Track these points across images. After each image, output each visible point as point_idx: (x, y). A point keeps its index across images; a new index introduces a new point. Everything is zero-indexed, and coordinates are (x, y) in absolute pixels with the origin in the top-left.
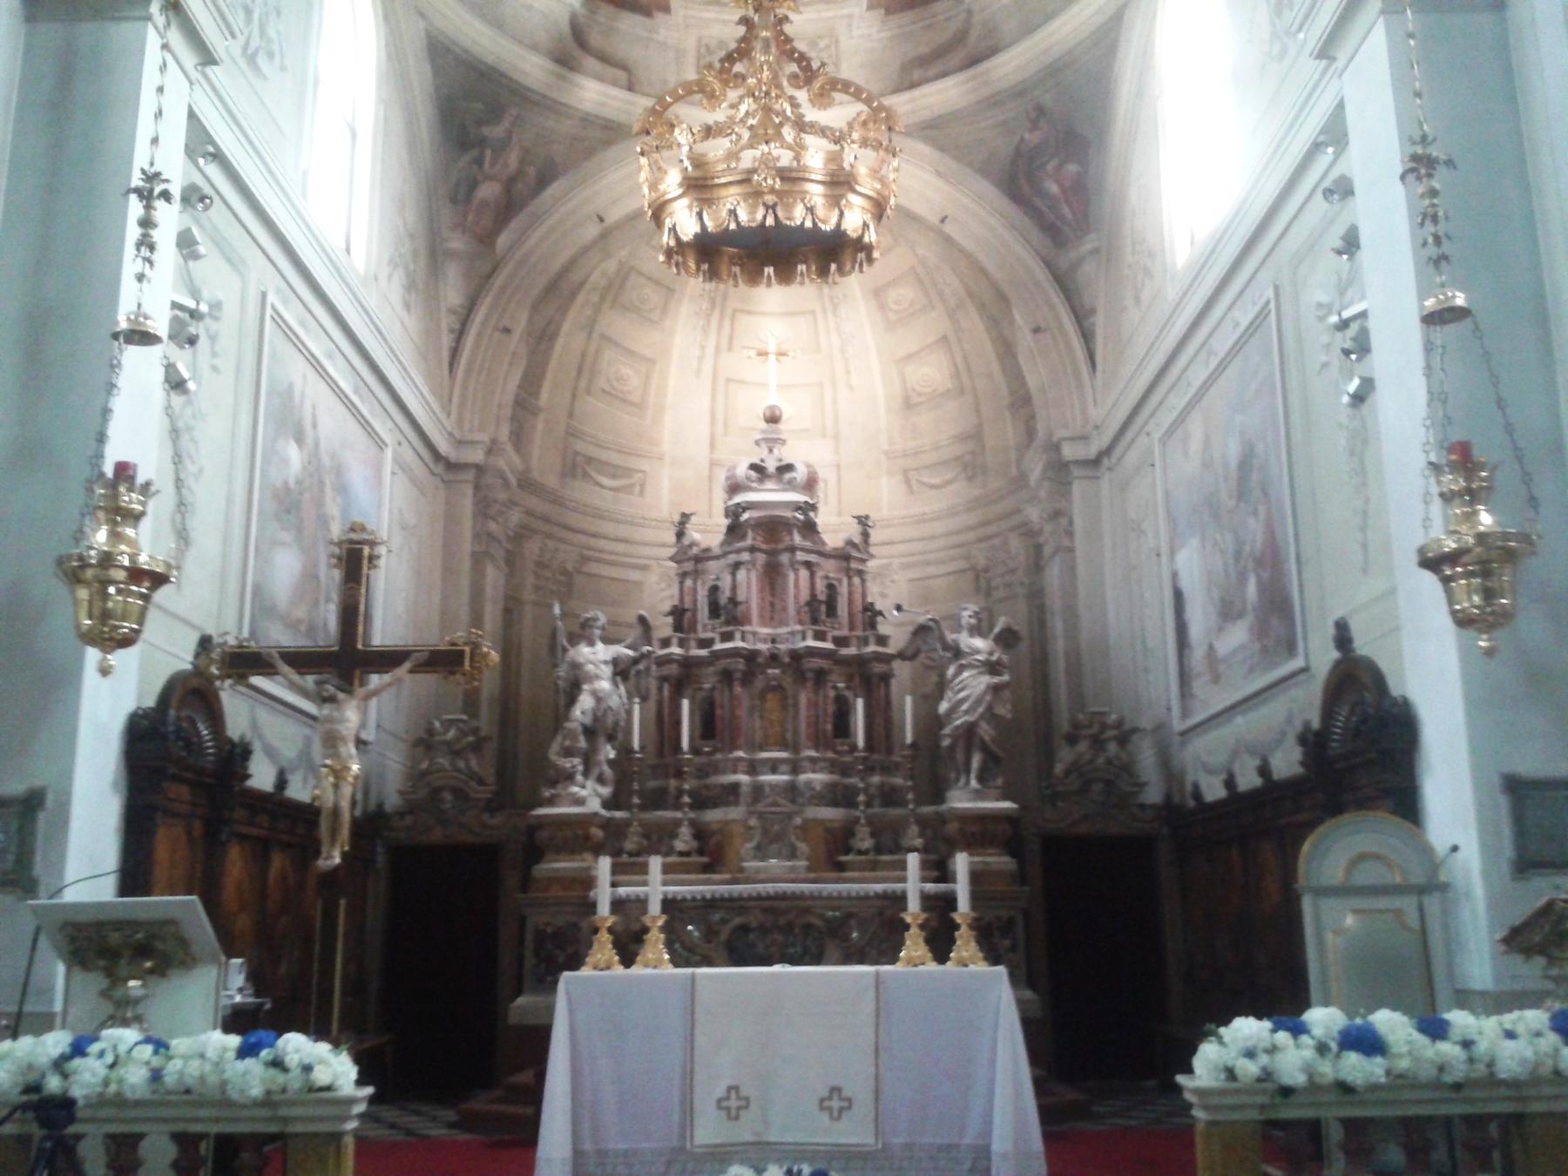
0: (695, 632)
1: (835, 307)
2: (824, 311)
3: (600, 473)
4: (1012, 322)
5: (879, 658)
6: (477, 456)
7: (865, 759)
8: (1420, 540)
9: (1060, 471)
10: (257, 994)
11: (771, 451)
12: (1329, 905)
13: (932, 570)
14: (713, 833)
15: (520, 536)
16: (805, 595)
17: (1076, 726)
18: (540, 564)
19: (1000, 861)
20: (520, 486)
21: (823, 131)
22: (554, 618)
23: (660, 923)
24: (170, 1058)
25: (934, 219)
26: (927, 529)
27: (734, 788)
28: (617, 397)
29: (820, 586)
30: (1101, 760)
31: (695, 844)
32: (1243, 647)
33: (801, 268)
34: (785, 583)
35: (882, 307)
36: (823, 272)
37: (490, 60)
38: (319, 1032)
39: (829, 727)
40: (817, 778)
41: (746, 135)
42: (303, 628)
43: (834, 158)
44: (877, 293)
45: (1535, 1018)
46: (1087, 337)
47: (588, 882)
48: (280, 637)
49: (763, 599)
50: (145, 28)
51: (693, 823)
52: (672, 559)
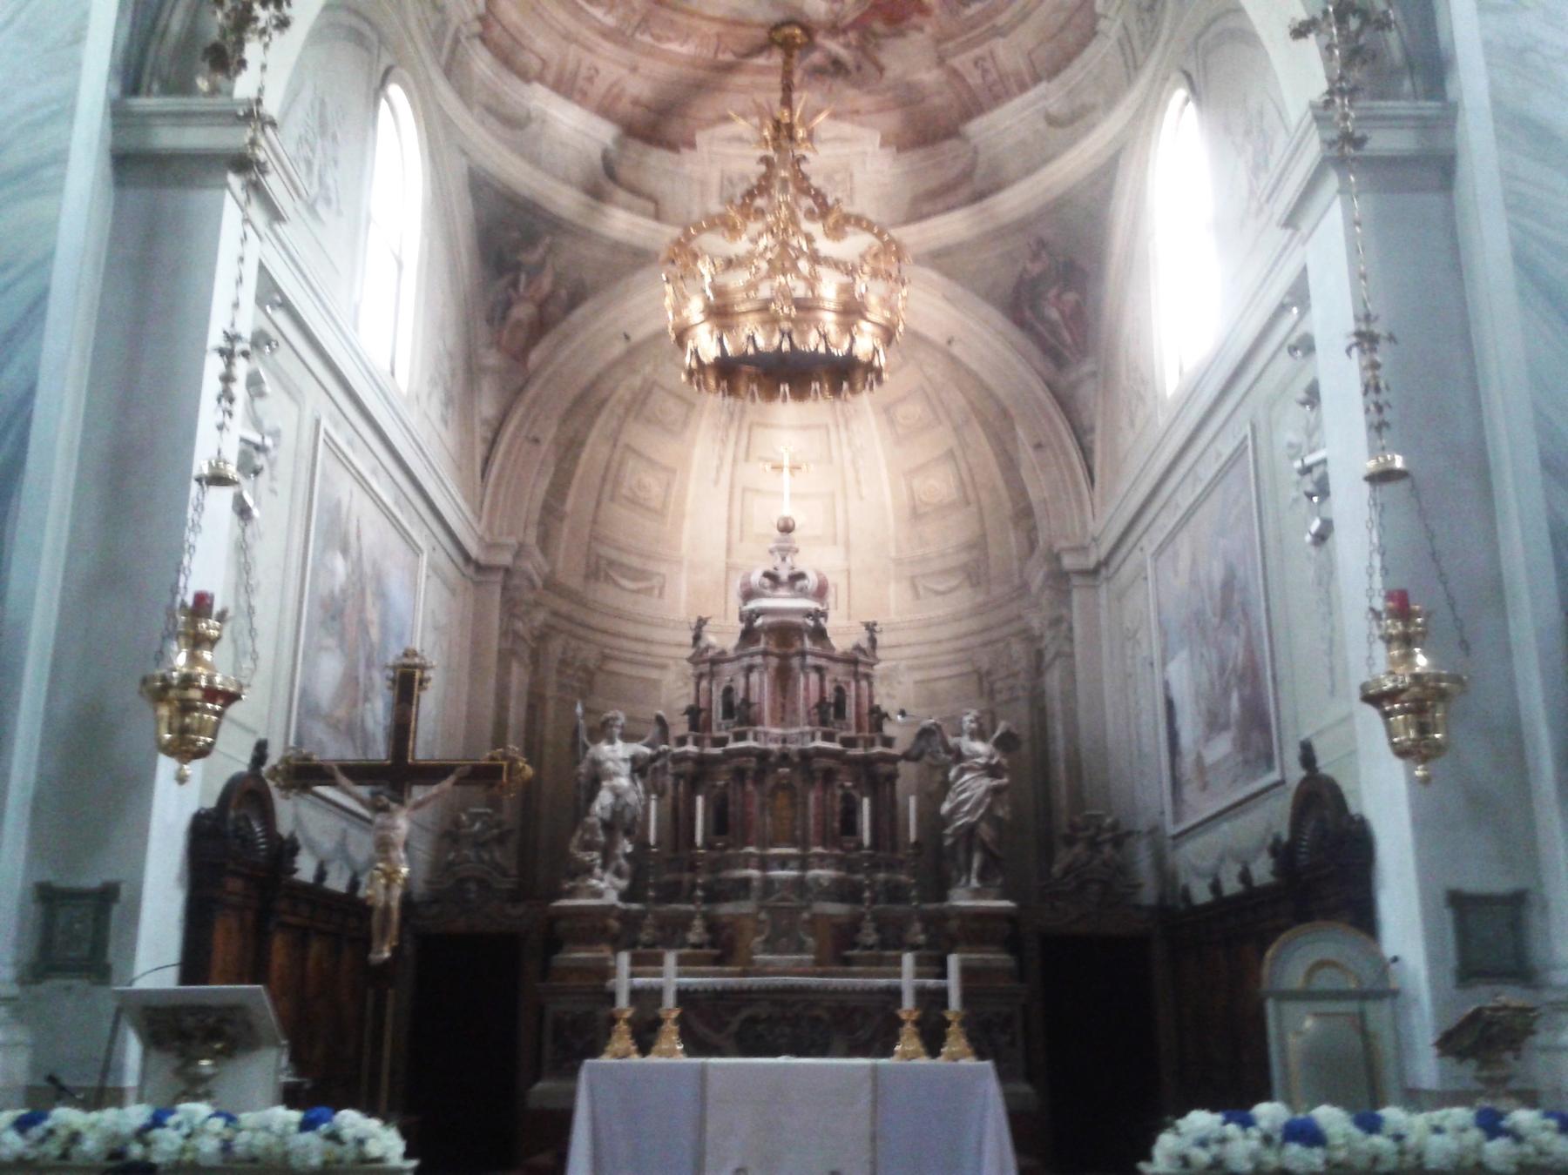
3: (623, 576)
4: (1014, 439)
5: (885, 758)
6: (505, 558)
7: (871, 856)
8: (1364, 677)
9: (1060, 580)
10: (297, 1074)
11: (784, 559)
12: (1290, 1008)
13: (935, 673)
15: (543, 637)
16: (814, 698)
17: (1073, 826)
18: (563, 662)
19: (998, 958)
21: (836, 264)
22: (576, 716)
23: (674, 1015)
24: (240, 1130)
25: (942, 341)
27: (746, 882)
29: (829, 688)
31: (707, 937)
32: (1226, 758)
33: (815, 386)
35: (891, 422)
36: (836, 390)
37: (525, 192)
38: (370, 1110)
39: (837, 825)
40: (823, 874)
41: (764, 266)
42: (342, 727)
43: (847, 289)
44: (887, 410)
45: (1460, 1115)
46: (1086, 453)
47: (606, 972)
48: (331, 749)
50: (223, 197)
51: (705, 916)
52: (690, 660)
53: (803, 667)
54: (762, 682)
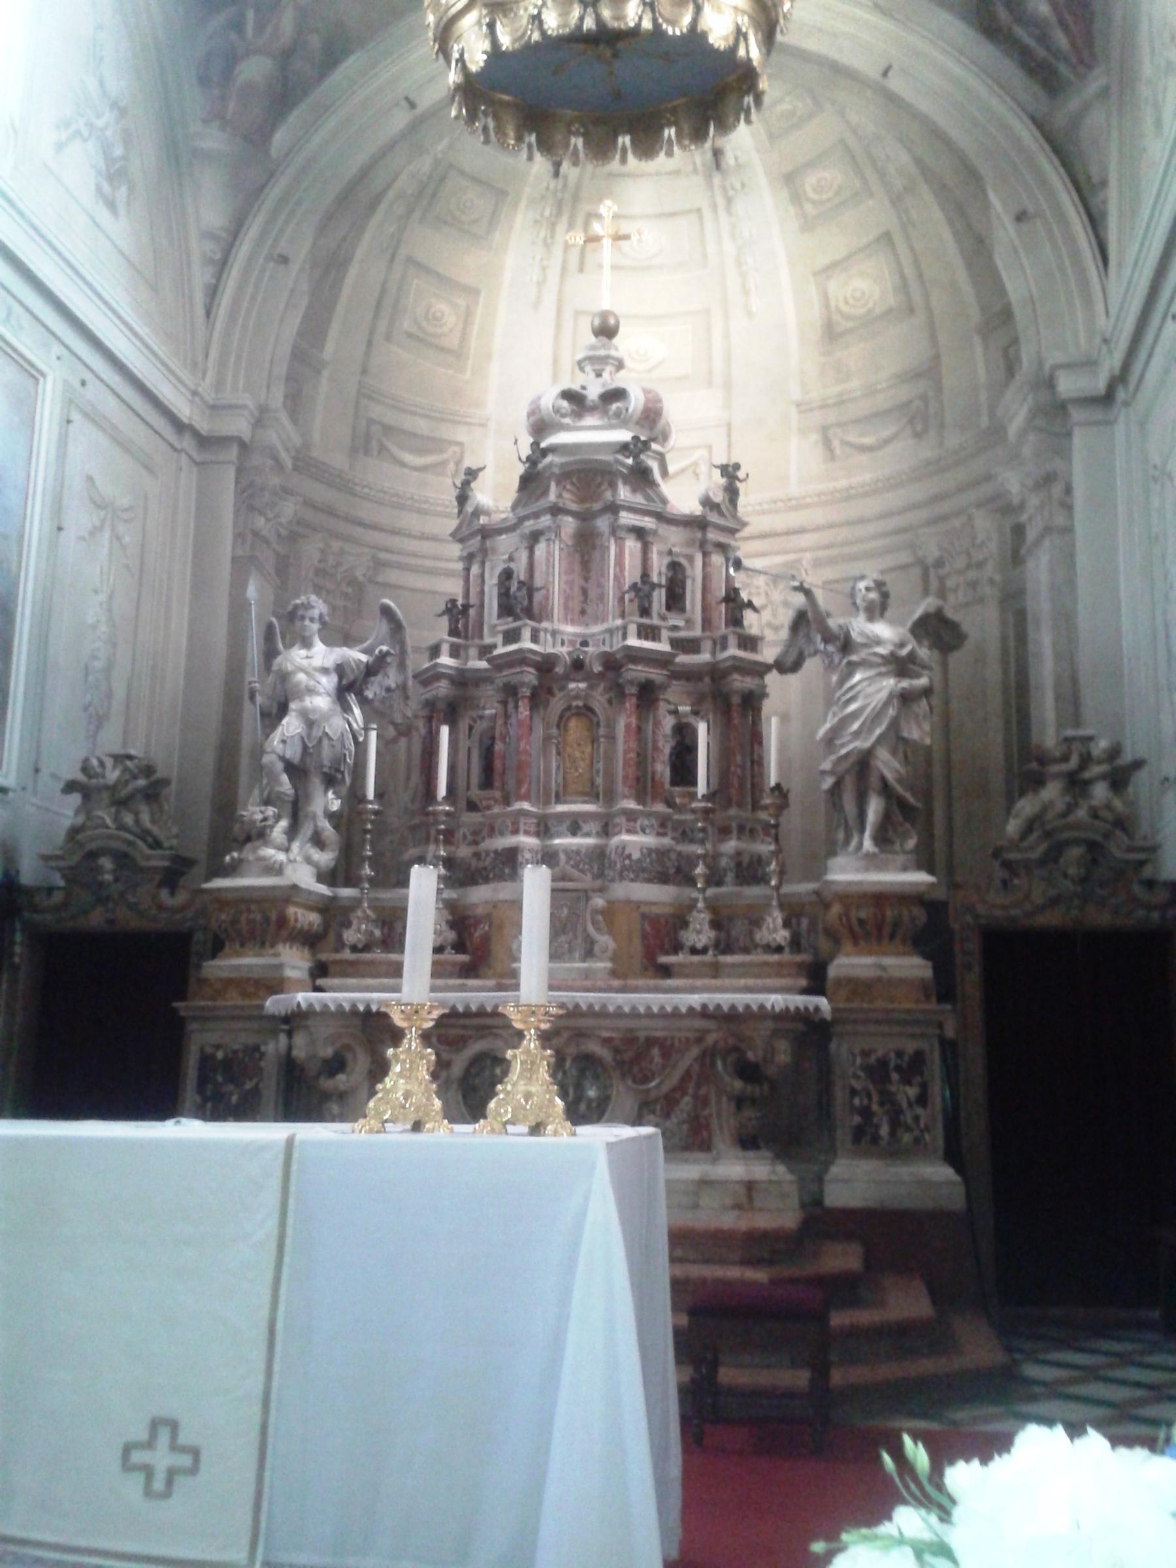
0: (481, 637)
1: (729, 201)
2: (714, 207)
4: (986, 206)
6: (240, 426)
9: (1054, 414)
14: (478, 921)
15: (294, 536)
16: (631, 575)
20: (296, 468)
25: (868, 67)
26: (854, 510)
28: (430, 345)
30: (1081, 813)
33: (670, 132)
34: (604, 558)
35: (797, 198)
40: (636, 841)
46: (1095, 221)
49: (570, 583)
53: (614, 530)
54: (550, 554)
